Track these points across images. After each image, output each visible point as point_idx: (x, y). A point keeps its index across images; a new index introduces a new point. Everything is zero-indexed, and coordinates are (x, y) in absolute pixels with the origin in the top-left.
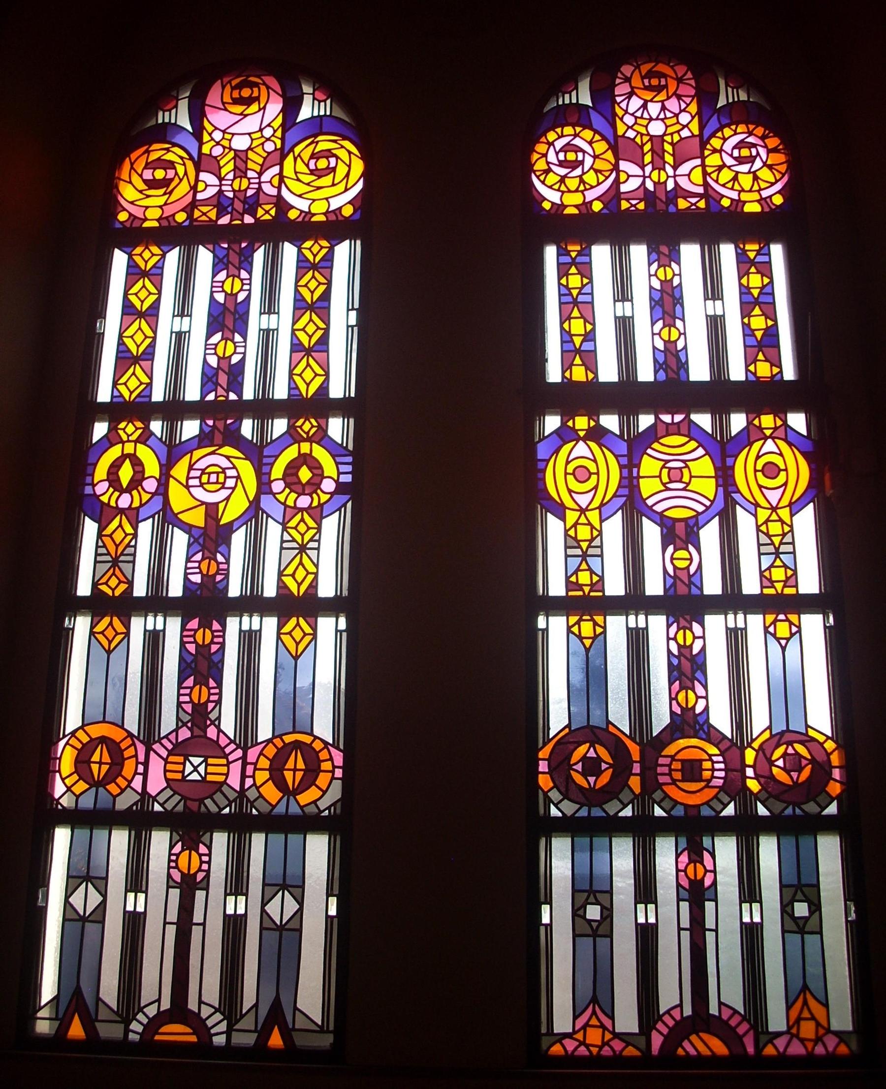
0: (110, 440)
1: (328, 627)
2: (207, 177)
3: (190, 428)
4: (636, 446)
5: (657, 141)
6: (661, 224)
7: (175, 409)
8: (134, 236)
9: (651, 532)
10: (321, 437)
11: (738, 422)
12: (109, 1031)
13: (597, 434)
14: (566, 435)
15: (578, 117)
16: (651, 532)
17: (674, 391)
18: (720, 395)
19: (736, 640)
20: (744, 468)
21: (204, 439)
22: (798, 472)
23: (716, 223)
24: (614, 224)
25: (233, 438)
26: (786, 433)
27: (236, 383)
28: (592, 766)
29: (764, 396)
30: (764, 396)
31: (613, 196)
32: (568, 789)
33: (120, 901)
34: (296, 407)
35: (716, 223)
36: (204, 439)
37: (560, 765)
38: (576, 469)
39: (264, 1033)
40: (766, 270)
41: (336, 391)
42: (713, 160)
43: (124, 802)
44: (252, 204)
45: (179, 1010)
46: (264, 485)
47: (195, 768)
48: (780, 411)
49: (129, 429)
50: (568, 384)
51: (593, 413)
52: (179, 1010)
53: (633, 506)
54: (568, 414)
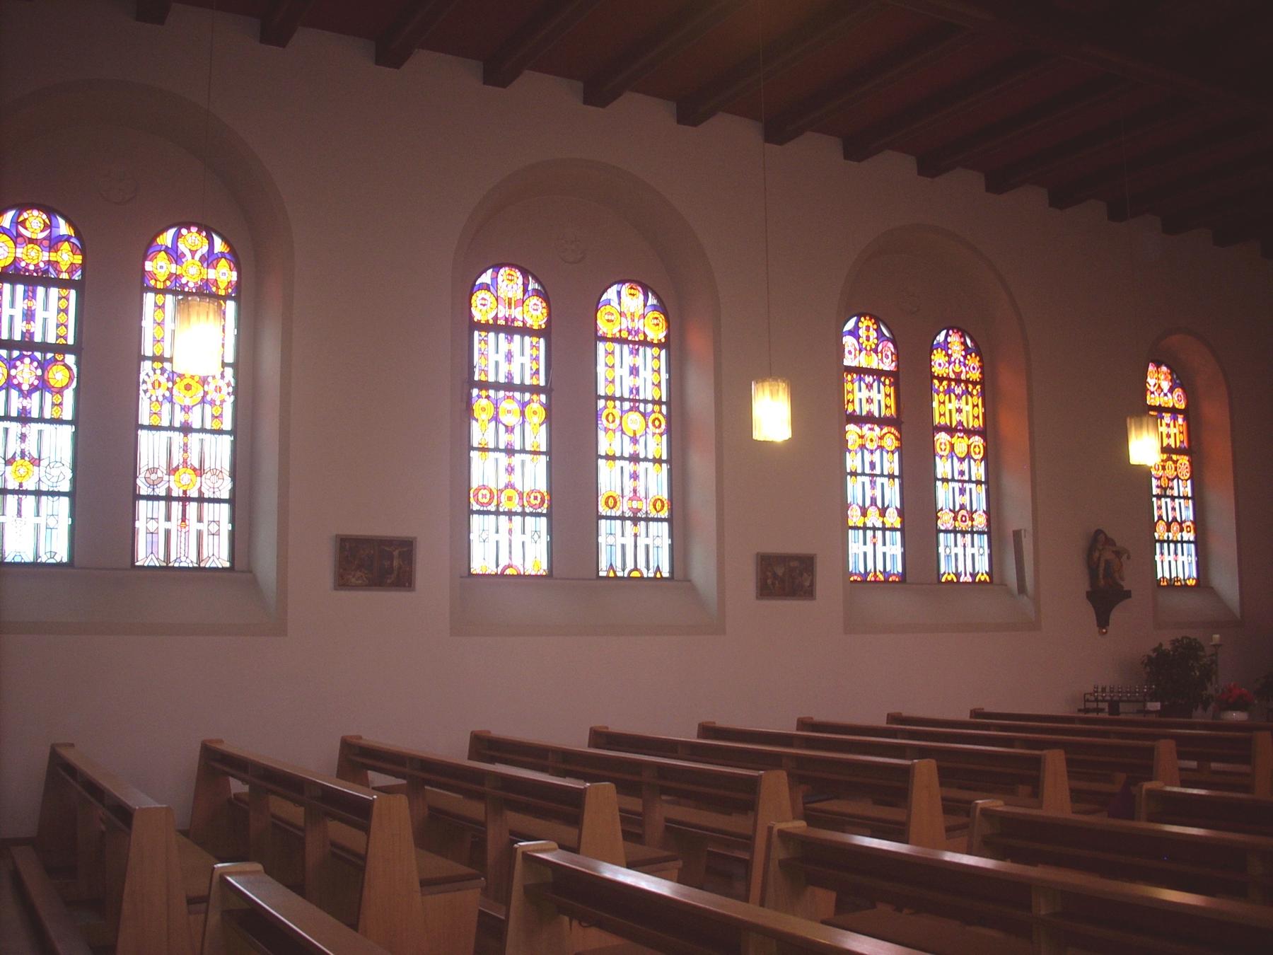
0: (606, 407)
1: (664, 465)
2: (623, 319)
3: (627, 405)
4: (44, 365)
5: (510, 299)
6: (509, 329)
7: (622, 399)
8: (604, 339)
9: (177, 408)
10: (660, 412)
11: (49, 356)
12: (620, 574)
13: (488, 397)
14: (479, 397)
15: (486, 287)
16: (502, 428)
17: (509, 386)
18: (523, 388)
19: (523, 463)
20: (528, 410)
21: (631, 409)
22: (542, 414)
23: (526, 331)
24: (493, 327)
25: (637, 409)
26: (660, 412)
27: (638, 393)
28: (484, 496)
29: (535, 390)
30: (535, 390)
31: (496, 318)
32: (477, 501)
33: (620, 540)
34: (654, 402)
35: (526, 331)
36: (631, 409)
37: (476, 495)
38: (482, 406)
39: (608, 572)
40: (538, 349)
41: (664, 399)
42: (526, 308)
43: (619, 513)
44: (637, 332)
45: (636, 569)
46: (647, 426)
47: (635, 504)
48: (538, 394)
49: (610, 403)
50: (480, 381)
51: (487, 389)
52: (636, 569)
53: (496, 418)
54: (480, 389)
